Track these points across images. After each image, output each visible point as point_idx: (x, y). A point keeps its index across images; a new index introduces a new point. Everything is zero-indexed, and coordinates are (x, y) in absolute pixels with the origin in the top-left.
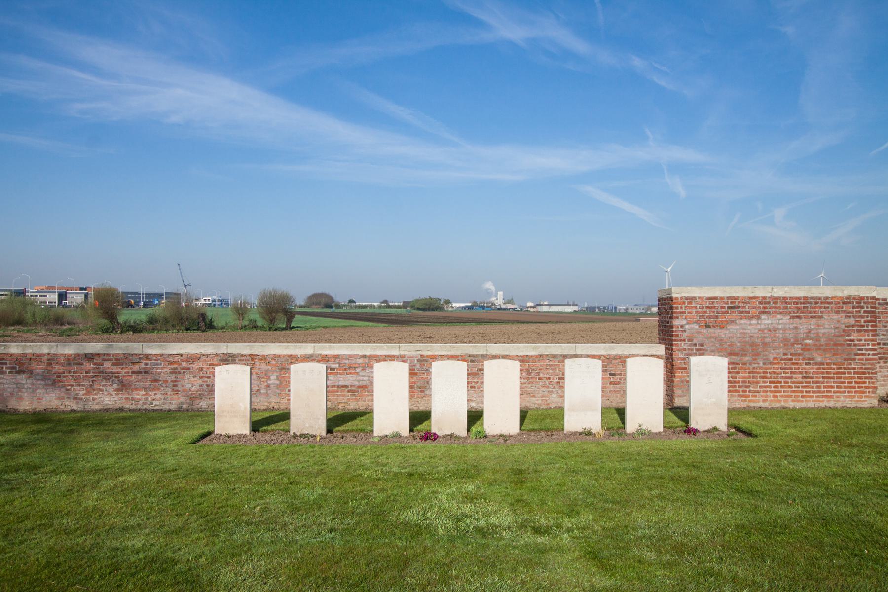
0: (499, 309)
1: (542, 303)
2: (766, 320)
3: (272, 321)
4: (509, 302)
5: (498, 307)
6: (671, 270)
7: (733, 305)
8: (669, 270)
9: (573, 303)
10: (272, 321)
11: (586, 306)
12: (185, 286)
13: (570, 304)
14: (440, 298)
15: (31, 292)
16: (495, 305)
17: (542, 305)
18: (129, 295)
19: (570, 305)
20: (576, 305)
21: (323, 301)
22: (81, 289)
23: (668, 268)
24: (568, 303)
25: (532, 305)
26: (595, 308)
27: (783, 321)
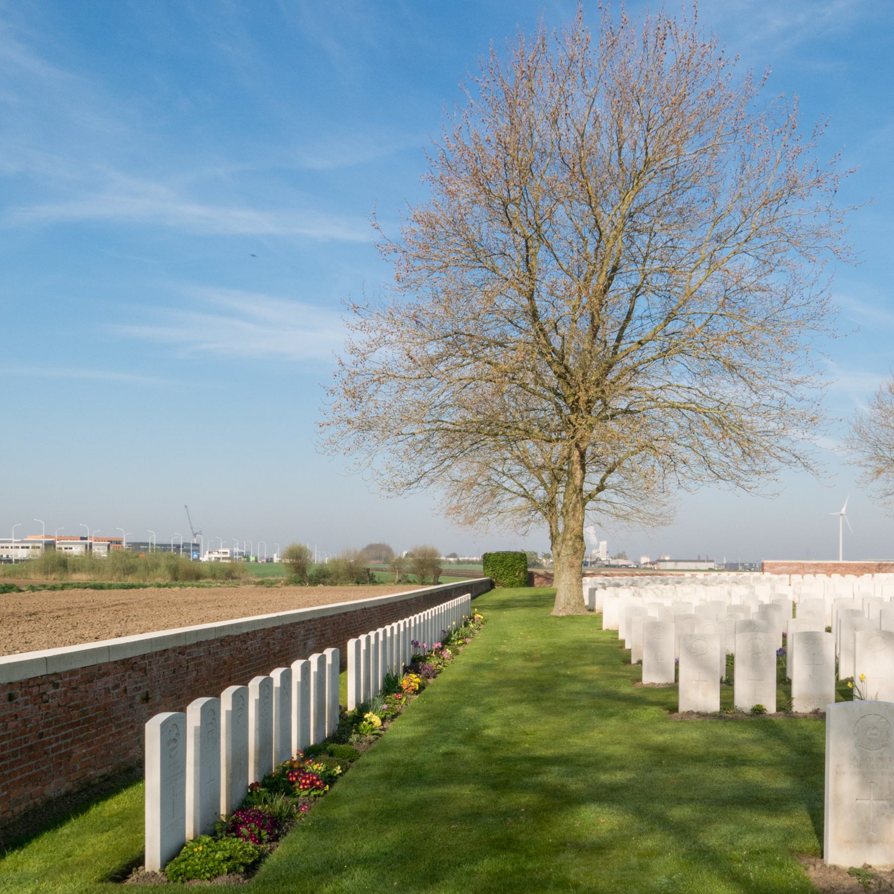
0: (607, 566)
1: (662, 558)
2: (782, 567)
3: (423, 576)
4: (620, 556)
5: (607, 563)
6: (846, 510)
7: (776, 564)
8: (843, 511)
9: (707, 558)
10: (423, 576)
11: (725, 562)
12: (195, 535)
13: (701, 559)
14: (536, 551)
15: (15, 542)
16: (600, 560)
17: (664, 561)
18: (142, 547)
19: (704, 561)
20: (712, 561)
21: (384, 554)
22: (82, 538)
23: (841, 511)
24: (699, 557)
25: (648, 560)
26: (738, 564)
27: (786, 567)
